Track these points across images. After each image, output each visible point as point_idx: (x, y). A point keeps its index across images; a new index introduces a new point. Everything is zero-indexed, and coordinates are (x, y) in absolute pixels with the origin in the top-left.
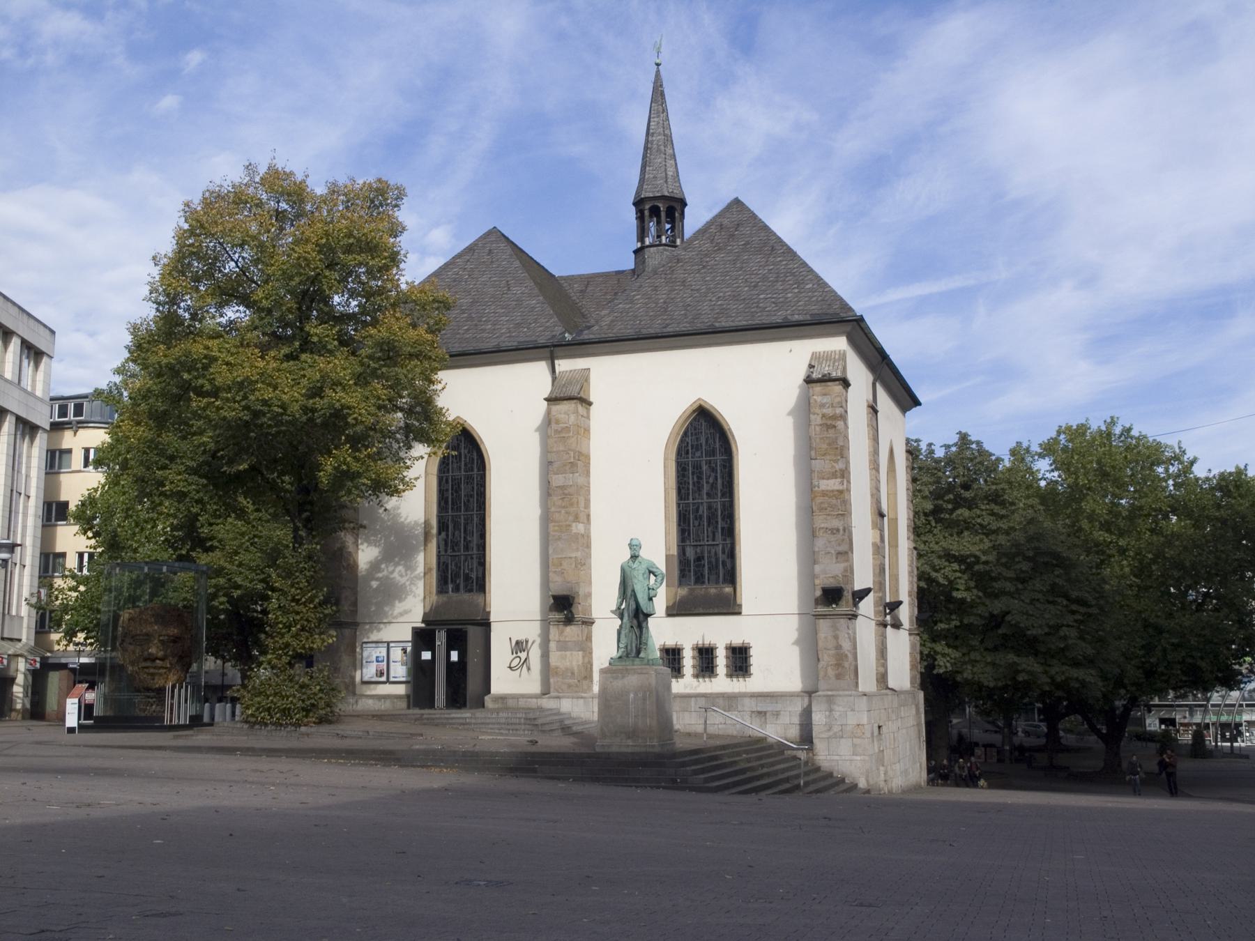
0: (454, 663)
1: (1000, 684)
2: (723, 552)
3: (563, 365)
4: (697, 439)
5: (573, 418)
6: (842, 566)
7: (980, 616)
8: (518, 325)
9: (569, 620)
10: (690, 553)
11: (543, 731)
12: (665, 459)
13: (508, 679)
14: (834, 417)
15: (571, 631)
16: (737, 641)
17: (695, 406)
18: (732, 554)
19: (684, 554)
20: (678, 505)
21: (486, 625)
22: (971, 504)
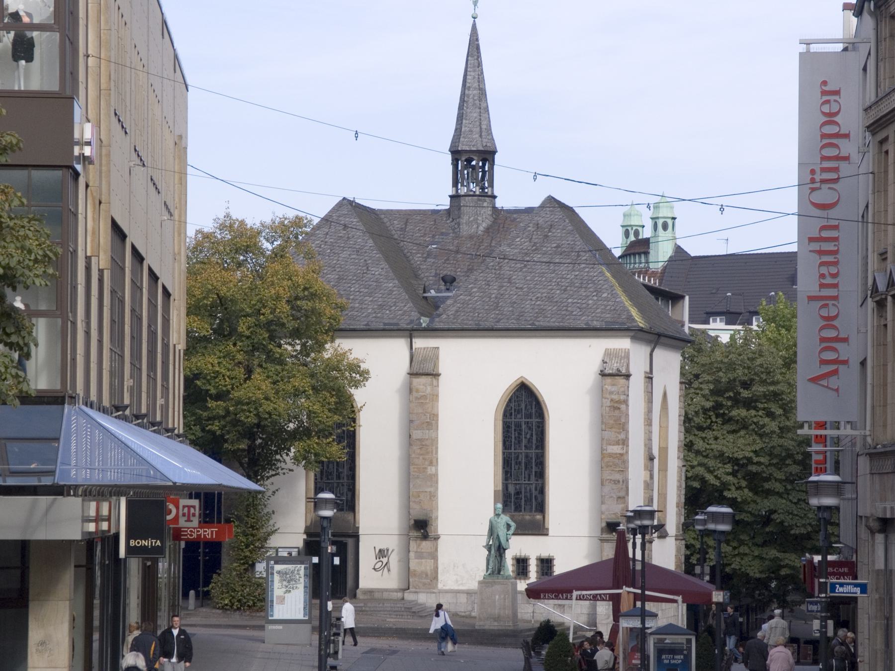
0: (336, 566)
1: (764, 576)
2: (536, 489)
3: (420, 343)
4: (519, 405)
5: (429, 388)
6: (621, 506)
7: (750, 513)
8: (381, 307)
9: (425, 537)
10: (512, 489)
11: (421, 617)
12: (495, 420)
13: (370, 577)
14: (619, 402)
15: (426, 545)
16: (545, 555)
17: (519, 382)
18: (542, 491)
19: (507, 489)
20: (504, 453)
21: (356, 537)
22: (749, 404)
